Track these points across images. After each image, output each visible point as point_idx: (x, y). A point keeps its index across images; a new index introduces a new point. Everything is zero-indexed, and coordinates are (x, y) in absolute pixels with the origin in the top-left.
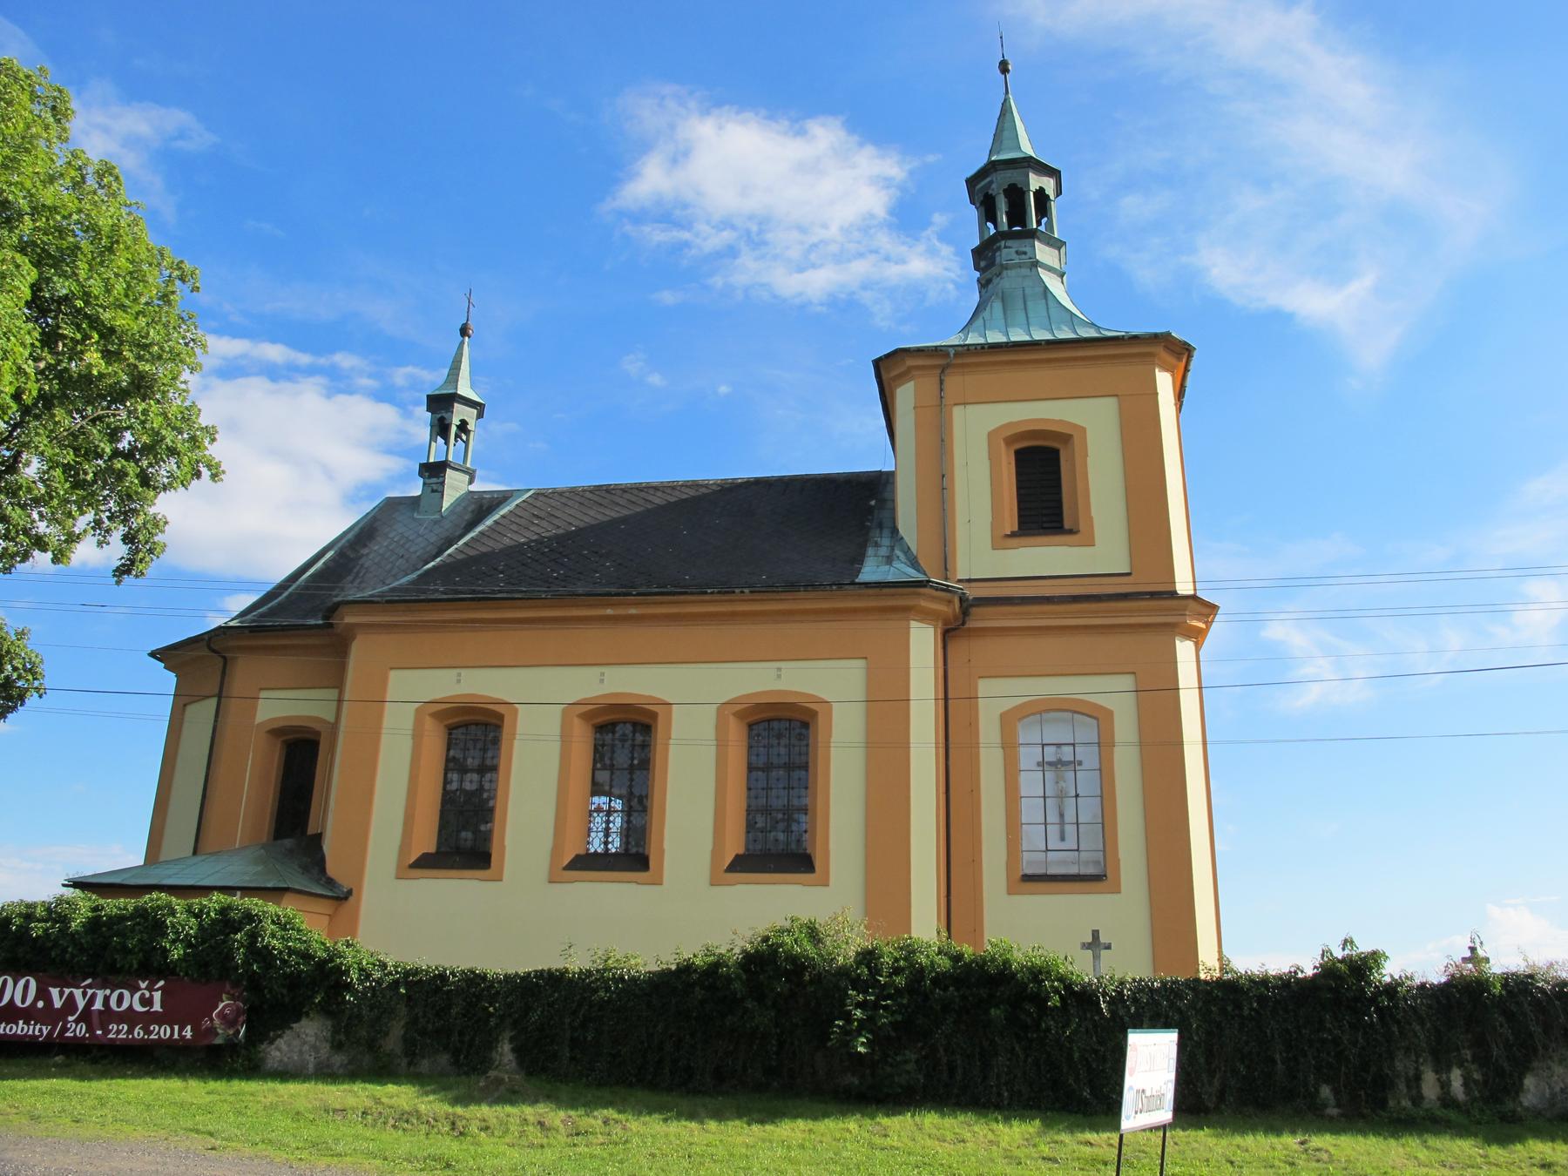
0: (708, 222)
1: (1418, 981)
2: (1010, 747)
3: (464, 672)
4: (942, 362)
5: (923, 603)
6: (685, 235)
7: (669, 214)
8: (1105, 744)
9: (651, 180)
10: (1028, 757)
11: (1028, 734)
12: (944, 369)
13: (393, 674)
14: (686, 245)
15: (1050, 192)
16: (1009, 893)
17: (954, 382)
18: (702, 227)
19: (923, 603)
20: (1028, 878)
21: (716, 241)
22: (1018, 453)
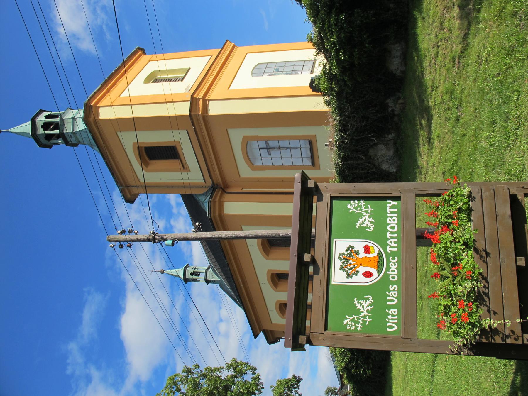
0: (96, 19)
1: (339, 161)
2: (263, 168)
3: (269, 309)
4: (126, 189)
5: (217, 214)
6: (104, 27)
7: (98, 35)
8: (257, 138)
9: (87, 45)
10: (267, 162)
11: (258, 163)
12: (127, 187)
13: (273, 322)
14: (107, 25)
15: (47, 114)
16: (322, 200)
17: (131, 181)
18: (99, 22)
19: (217, 214)
20: (313, 164)
21: (102, 16)
22: (151, 158)
